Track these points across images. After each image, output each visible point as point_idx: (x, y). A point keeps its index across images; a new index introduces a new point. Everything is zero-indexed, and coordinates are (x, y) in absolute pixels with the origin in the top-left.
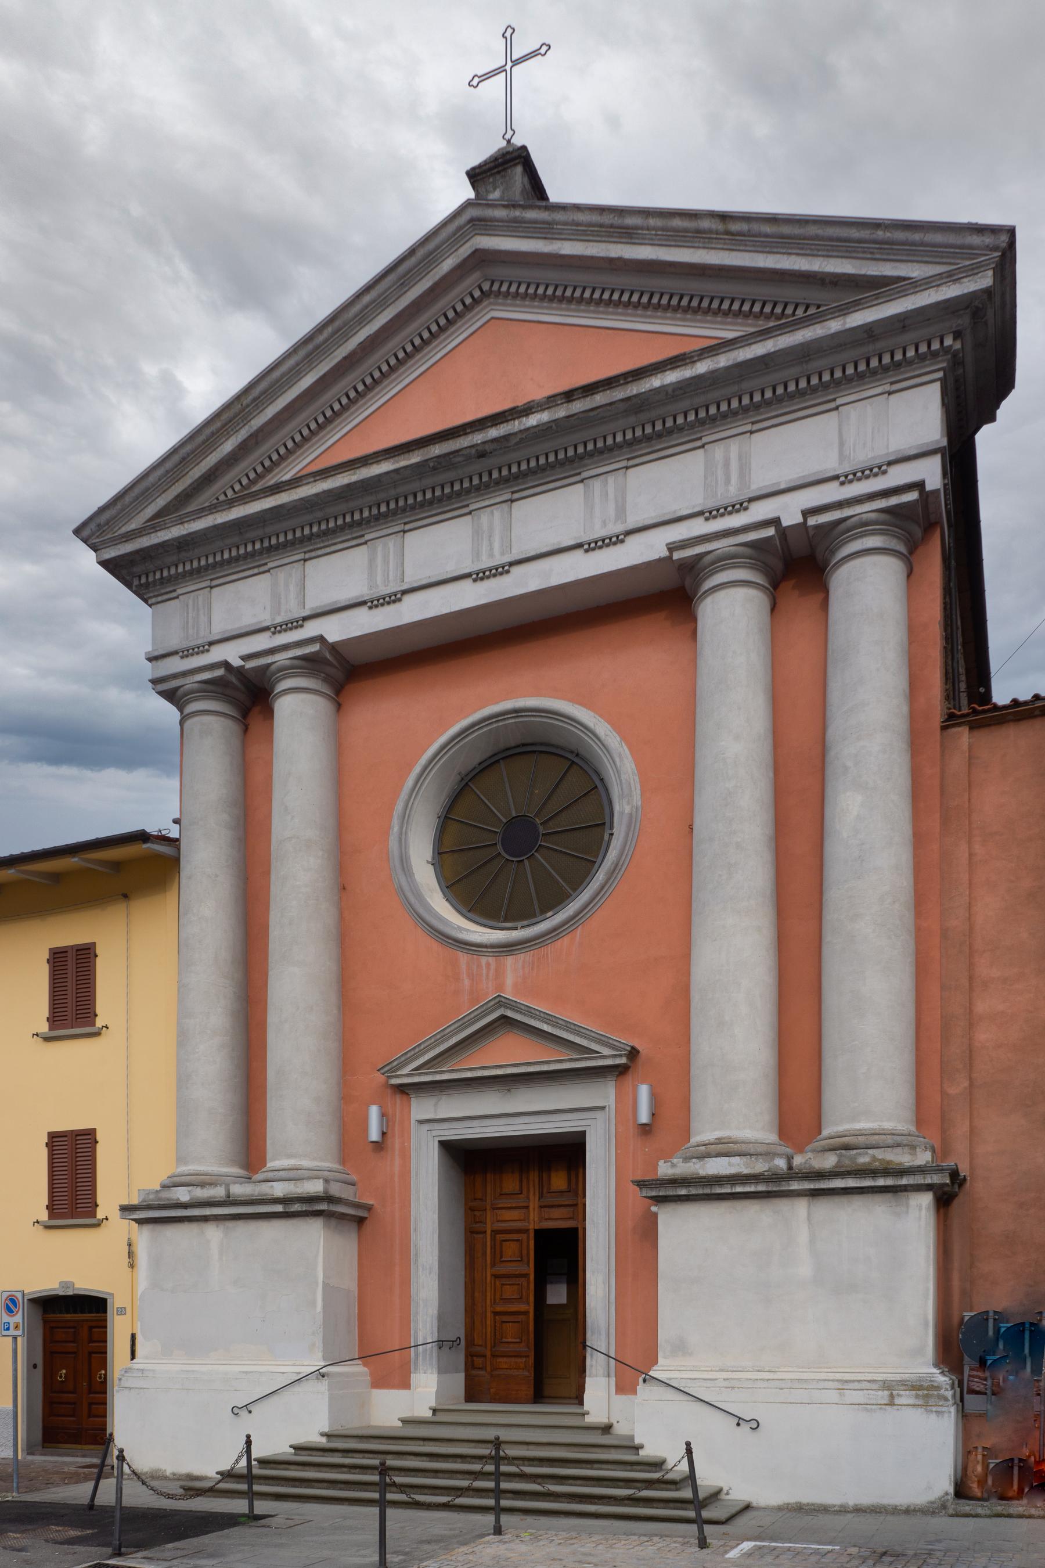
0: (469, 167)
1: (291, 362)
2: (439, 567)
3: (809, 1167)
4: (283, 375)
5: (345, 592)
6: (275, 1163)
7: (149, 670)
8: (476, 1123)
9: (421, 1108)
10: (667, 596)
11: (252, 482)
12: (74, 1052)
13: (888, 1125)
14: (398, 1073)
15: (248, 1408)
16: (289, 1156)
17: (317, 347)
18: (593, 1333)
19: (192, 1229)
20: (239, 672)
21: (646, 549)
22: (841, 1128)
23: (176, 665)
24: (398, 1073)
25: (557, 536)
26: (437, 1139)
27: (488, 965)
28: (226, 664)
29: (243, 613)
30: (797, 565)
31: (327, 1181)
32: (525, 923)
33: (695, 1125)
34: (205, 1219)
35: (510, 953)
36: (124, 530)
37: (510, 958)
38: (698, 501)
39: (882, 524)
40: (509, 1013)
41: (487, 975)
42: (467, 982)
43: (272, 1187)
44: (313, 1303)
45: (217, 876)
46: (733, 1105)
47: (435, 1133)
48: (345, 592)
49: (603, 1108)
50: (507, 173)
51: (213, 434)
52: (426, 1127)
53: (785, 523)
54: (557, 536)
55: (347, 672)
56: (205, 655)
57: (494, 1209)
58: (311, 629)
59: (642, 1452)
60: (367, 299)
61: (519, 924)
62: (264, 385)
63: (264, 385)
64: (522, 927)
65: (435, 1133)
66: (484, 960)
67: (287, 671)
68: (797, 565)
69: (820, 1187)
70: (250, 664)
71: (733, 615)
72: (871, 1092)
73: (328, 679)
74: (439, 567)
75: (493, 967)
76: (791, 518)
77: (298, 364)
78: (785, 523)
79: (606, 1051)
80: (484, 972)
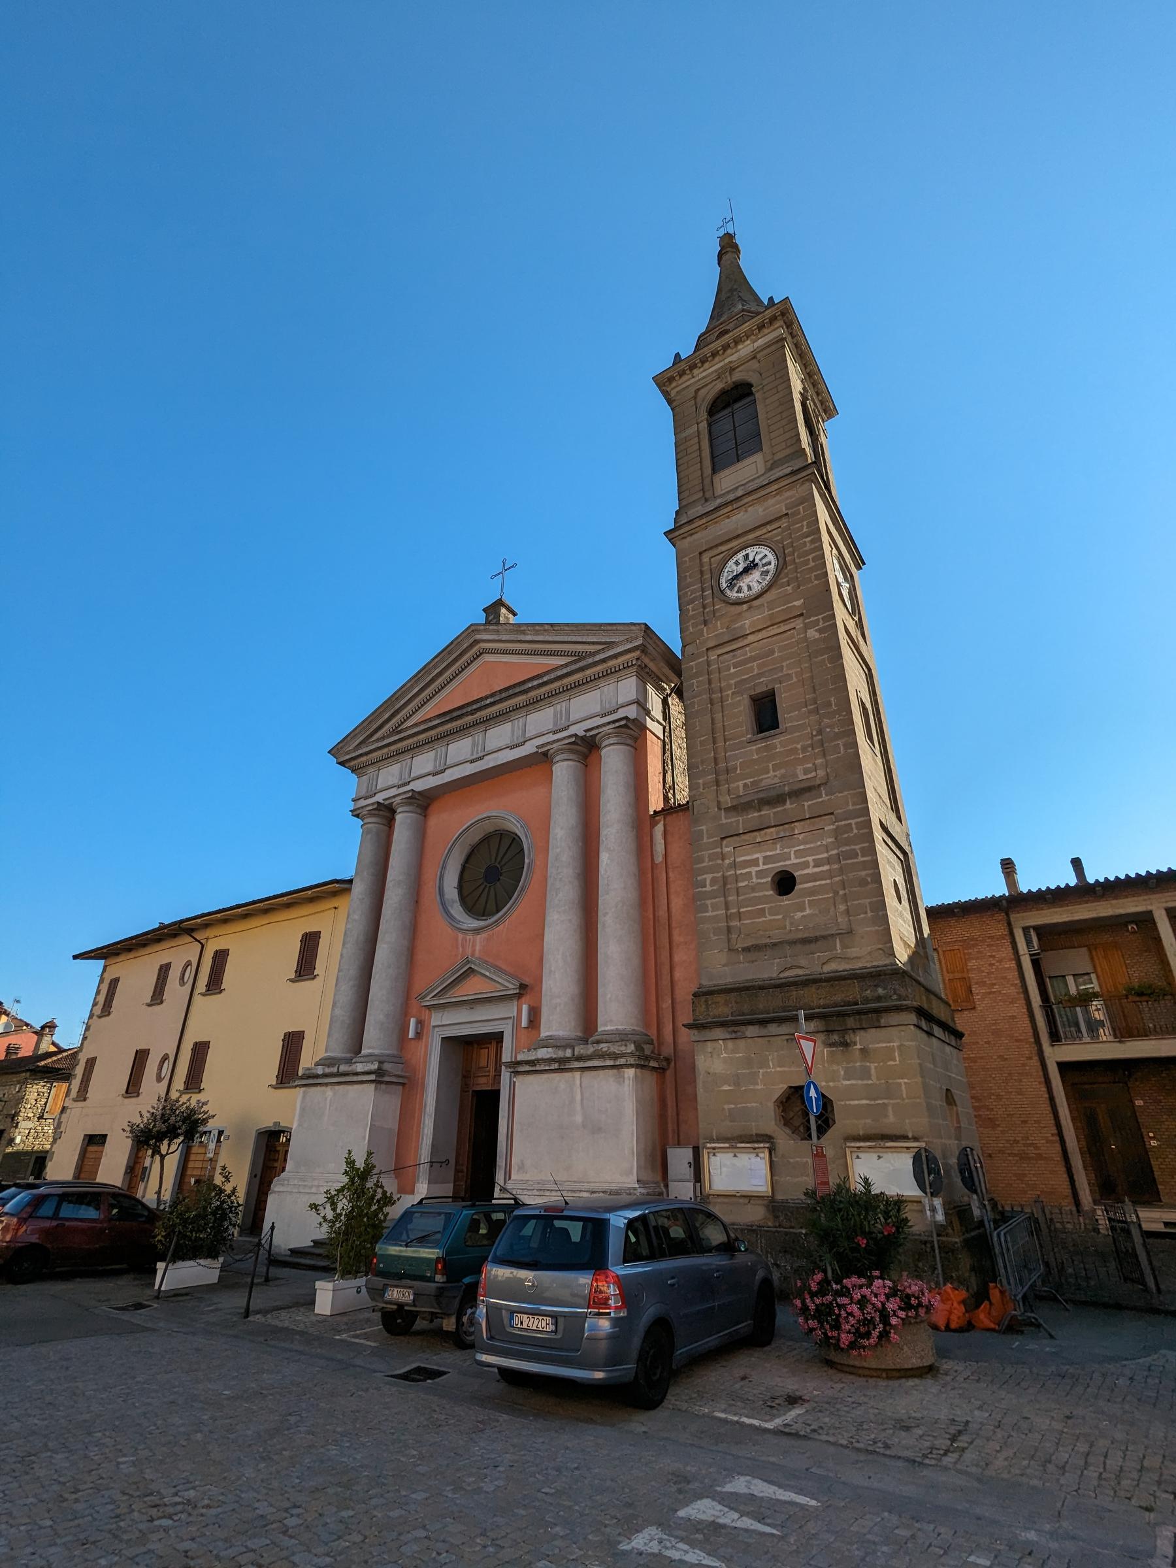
2: (460, 756)
3: (584, 1051)
5: (423, 769)
7: (352, 806)
9: (436, 1019)
12: (306, 985)
13: (561, 1033)
20: (583, 738)
21: (529, 749)
22: (547, 1034)
23: (363, 803)
25: (501, 742)
28: (575, 735)
29: (389, 779)
30: (586, 748)
31: (380, 1063)
34: (326, 1084)
38: (597, 709)
46: (558, 1020)
48: (423, 769)
50: (493, 610)
54: (501, 742)
55: (424, 802)
58: (411, 787)
68: (586, 748)
70: (386, 803)
71: (563, 771)
72: (617, 1011)
73: (419, 806)
74: (460, 756)
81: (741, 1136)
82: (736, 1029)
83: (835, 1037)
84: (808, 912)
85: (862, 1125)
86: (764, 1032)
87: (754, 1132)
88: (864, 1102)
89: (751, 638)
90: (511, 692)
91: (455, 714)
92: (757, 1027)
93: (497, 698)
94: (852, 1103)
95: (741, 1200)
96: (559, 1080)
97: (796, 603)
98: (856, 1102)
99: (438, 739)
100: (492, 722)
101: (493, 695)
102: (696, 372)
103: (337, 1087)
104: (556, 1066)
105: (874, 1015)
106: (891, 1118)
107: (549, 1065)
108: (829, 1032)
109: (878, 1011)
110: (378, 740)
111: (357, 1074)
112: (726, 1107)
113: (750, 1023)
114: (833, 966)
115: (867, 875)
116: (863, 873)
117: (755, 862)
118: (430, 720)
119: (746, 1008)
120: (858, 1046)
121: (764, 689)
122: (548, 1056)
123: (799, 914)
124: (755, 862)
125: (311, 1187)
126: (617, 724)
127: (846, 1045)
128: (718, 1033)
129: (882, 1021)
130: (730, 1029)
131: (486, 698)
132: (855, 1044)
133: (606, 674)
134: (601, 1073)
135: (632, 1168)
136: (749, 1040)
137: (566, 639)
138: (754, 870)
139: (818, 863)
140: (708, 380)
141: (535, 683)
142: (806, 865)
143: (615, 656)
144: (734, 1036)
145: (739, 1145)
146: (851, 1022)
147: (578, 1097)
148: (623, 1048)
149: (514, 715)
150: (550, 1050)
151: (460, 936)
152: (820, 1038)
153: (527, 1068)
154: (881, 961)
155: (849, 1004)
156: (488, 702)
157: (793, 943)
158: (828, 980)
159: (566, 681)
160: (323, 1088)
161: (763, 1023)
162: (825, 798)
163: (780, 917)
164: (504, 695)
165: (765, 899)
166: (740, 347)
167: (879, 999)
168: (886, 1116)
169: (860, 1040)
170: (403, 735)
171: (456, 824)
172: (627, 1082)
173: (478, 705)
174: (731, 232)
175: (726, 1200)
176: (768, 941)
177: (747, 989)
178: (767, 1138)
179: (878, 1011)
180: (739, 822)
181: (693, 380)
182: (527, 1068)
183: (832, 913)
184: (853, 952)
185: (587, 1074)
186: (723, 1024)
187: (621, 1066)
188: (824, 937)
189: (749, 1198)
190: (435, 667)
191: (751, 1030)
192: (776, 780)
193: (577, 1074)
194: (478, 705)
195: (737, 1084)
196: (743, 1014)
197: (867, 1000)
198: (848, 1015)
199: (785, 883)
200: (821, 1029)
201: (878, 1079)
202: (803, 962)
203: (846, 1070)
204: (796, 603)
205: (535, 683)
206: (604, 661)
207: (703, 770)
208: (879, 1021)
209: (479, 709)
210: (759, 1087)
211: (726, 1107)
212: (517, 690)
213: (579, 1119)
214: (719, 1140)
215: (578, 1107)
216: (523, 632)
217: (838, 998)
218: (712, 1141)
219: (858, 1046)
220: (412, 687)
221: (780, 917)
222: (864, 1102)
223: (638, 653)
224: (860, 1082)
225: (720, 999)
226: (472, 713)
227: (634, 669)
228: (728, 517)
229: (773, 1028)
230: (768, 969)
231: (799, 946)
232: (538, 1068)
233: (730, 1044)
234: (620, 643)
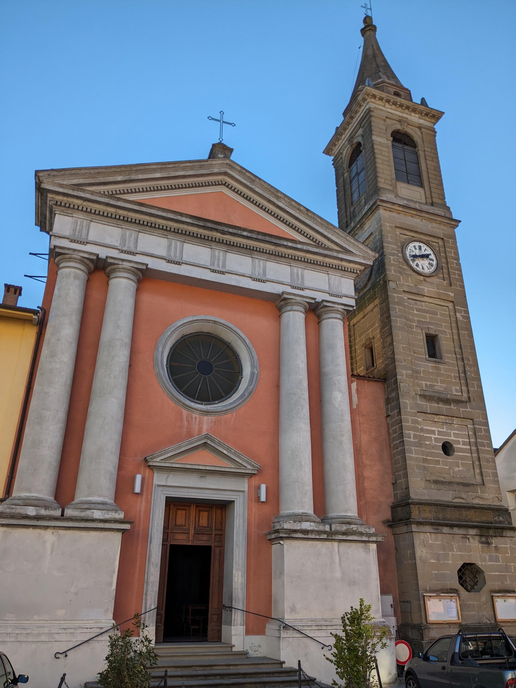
0: (234, 151)
1: (155, 167)
3: (326, 527)
4: (150, 169)
6: (81, 496)
8: (186, 490)
9: (159, 479)
10: (278, 303)
11: (117, 194)
14: (155, 460)
15: (65, 654)
16: (100, 496)
17: (166, 168)
18: (236, 602)
19: (38, 531)
24: (155, 460)
26: (165, 495)
27: (196, 418)
32: (206, 403)
33: (77, 495)
34: (46, 527)
35: (206, 415)
36: (61, 182)
37: (205, 417)
39: (78, 260)
40: (209, 442)
41: (195, 422)
42: (186, 423)
43: (93, 512)
44: (111, 584)
45: (72, 343)
46: (299, 499)
47: (165, 492)
49: (243, 491)
51: (115, 172)
52: (161, 489)
53: (149, 266)
56: (83, 246)
57: (172, 533)
59: (284, 666)
60: (188, 164)
61: (204, 403)
62: (142, 168)
63: (142, 168)
64: (205, 404)
65: (165, 492)
66: (194, 415)
67: (125, 270)
69: (330, 536)
75: (198, 419)
76: (103, 256)
77: (157, 168)
78: (149, 266)
79: (249, 467)
80: (194, 421)
81: (442, 589)
82: (437, 527)
83: (483, 539)
84: (461, 468)
85: (436, 584)
86: (451, 531)
87: (449, 587)
88: (498, 573)
89: (425, 299)
90: (267, 238)
91: (210, 225)
92: (448, 528)
93: (255, 236)
94: (494, 573)
95: (446, 626)
96: (323, 548)
97: (450, 294)
98: (494, 573)
99: (176, 232)
100: (235, 249)
101: (251, 231)
102: (387, 105)
103: (62, 532)
104: (325, 536)
105: (500, 530)
106: (508, 582)
107: (319, 535)
108: (481, 536)
109: (503, 528)
110: (93, 193)
111: (93, 520)
112: (433, 572)
113: (446, 525)
114: (476, 501)
115: (490, 458)
116: (488, 456)
117: (433, 432)
118: (181, 214)
119: (441, 516)
120: (494, 545)
121: (434, 333)
122: (311, 528)
123: (457, 469)
124: (433, 432)
125: (39, 635)
126: (346, 308)
127: (488, 544)
128: (428, 528)
129: (504, 534)
130: (434, 527)
131: (244, 230)
132: (492, 544)
133: (337, 268)
134: (353, 544)
135: (379, 609)
136: (444, 535)
137: (314, 226)
138: (433, 436)
139: (464, 444)
140: (394, 117)
141: (290, 244)
142: (458, 442)
143: (350, 261)
144: (436, 531)
145: (442, 594)
146: (491, 532)
147: (337, 560)
148: (367, 530)
149: (256, 255)
150: (312, 524)
151: (185, 412)
152: (477, 538)
153: (301, 535)
154: (497, 503)
155: (488, 522)
156: (245, 234)
157: (459, 484)
158: (455, 507)
159: (327, 260)
160: (42, 532)
161: (452, 526)
162: (469, 410)
163: (448, 467)
164: (260, 237)
165: (437, 455)
166: (413, 114)
167: (501, 522)
168: (506, 581)
169: (495, 541)
170: (119, 204)
171: (189, 317)
172: (371, 552)
173: (234, 231)
174: (370, 15)
175: (438, 626)
176: (443, 479)
177: (441, 505)
178: (455, 591)
179: (503, 528)
180: (429, 406)
181: (382, 108)
182: (301, 535)
183: (393, 461)
184: (486, 495)
185: (343, 544)
186: (432, 524)
187: (369, 542)
188: (473, 485)
189: (450, 624)
190: (183, 169)
191: (446, 530)
192: (442, 389)
193: (336, 544)
194: (234, 231)
195: (438, 559)
196: (439, 520)
197: (496, 522)
198: (490, 528)
199: (447, 448)
200: (479, 534)
201: (503, 563)
202: (464, 496)
203: (490, 556)
204: (450, 294)
205: (290, 244)
206: (342, 260)
207: (405, 365)
208: (502, 534)
209: (212, 229)
210: (450, 562)
211: (433, 572)
212: (274, 240)
213: (338, 574)
214: (431, 591)
215: (337, 566)
216: (278, 198)
217: (484, 519)
218: (427, 592)
219: (494, 545)
220: (155, 171)
221: (448, 467)
222: (498, 573)
223: (363, 268)
224: (495, 563)
225: (427, 508)
226: (223, 233)
227: (355, 275)
228: (412, 217)
229: (456, 530)
230: (447, 496)
231: (461, 487)
232: (310, 536)
233: (433, 536)
234: (358, 256)
